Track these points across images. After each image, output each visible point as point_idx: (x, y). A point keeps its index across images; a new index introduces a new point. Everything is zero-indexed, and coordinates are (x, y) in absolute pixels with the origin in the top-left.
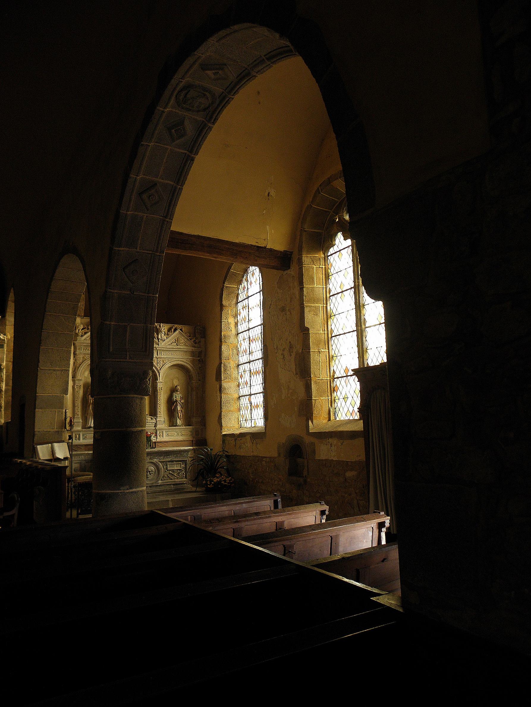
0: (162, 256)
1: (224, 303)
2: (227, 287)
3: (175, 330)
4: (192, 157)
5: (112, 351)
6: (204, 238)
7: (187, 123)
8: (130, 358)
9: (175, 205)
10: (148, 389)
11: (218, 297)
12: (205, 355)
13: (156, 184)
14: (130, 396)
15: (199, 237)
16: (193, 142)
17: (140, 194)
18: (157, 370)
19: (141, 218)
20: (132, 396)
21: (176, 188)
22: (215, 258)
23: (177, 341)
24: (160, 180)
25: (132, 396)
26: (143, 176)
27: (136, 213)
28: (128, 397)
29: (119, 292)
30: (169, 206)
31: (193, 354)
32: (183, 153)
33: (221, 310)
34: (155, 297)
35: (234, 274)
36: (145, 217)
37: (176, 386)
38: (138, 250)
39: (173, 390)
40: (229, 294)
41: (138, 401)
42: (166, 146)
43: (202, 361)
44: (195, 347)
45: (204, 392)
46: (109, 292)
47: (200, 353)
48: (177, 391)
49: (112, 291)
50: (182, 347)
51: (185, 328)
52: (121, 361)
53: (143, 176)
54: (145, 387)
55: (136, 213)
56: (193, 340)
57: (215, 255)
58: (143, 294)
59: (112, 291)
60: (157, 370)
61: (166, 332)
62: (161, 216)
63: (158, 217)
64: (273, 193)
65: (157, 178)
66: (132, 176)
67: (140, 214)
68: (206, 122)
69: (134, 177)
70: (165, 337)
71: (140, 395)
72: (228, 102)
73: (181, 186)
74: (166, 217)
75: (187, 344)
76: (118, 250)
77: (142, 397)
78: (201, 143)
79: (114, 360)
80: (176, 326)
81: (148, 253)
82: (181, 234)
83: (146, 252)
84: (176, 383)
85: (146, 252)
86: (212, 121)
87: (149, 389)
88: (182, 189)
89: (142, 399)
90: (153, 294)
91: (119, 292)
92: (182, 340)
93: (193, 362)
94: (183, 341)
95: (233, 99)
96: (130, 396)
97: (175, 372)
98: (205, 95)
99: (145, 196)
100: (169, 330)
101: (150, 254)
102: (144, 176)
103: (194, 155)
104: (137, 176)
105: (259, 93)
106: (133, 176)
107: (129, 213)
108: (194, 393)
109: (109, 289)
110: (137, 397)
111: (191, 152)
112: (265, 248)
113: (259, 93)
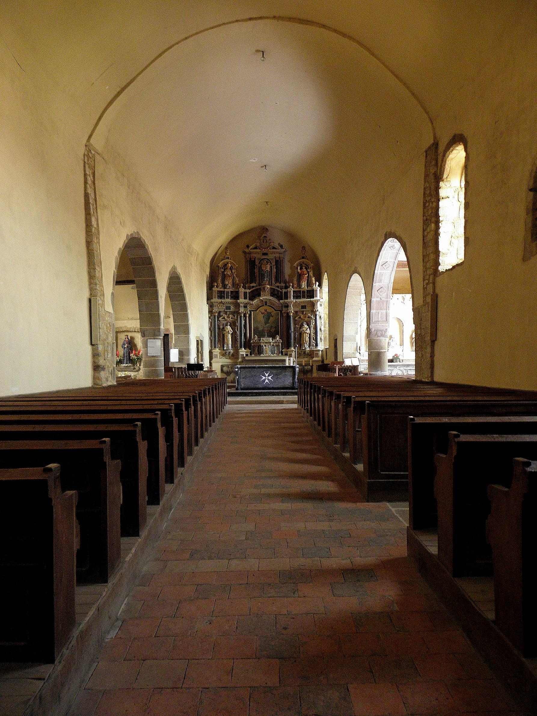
8: (381, 324)
38: (382, 284)
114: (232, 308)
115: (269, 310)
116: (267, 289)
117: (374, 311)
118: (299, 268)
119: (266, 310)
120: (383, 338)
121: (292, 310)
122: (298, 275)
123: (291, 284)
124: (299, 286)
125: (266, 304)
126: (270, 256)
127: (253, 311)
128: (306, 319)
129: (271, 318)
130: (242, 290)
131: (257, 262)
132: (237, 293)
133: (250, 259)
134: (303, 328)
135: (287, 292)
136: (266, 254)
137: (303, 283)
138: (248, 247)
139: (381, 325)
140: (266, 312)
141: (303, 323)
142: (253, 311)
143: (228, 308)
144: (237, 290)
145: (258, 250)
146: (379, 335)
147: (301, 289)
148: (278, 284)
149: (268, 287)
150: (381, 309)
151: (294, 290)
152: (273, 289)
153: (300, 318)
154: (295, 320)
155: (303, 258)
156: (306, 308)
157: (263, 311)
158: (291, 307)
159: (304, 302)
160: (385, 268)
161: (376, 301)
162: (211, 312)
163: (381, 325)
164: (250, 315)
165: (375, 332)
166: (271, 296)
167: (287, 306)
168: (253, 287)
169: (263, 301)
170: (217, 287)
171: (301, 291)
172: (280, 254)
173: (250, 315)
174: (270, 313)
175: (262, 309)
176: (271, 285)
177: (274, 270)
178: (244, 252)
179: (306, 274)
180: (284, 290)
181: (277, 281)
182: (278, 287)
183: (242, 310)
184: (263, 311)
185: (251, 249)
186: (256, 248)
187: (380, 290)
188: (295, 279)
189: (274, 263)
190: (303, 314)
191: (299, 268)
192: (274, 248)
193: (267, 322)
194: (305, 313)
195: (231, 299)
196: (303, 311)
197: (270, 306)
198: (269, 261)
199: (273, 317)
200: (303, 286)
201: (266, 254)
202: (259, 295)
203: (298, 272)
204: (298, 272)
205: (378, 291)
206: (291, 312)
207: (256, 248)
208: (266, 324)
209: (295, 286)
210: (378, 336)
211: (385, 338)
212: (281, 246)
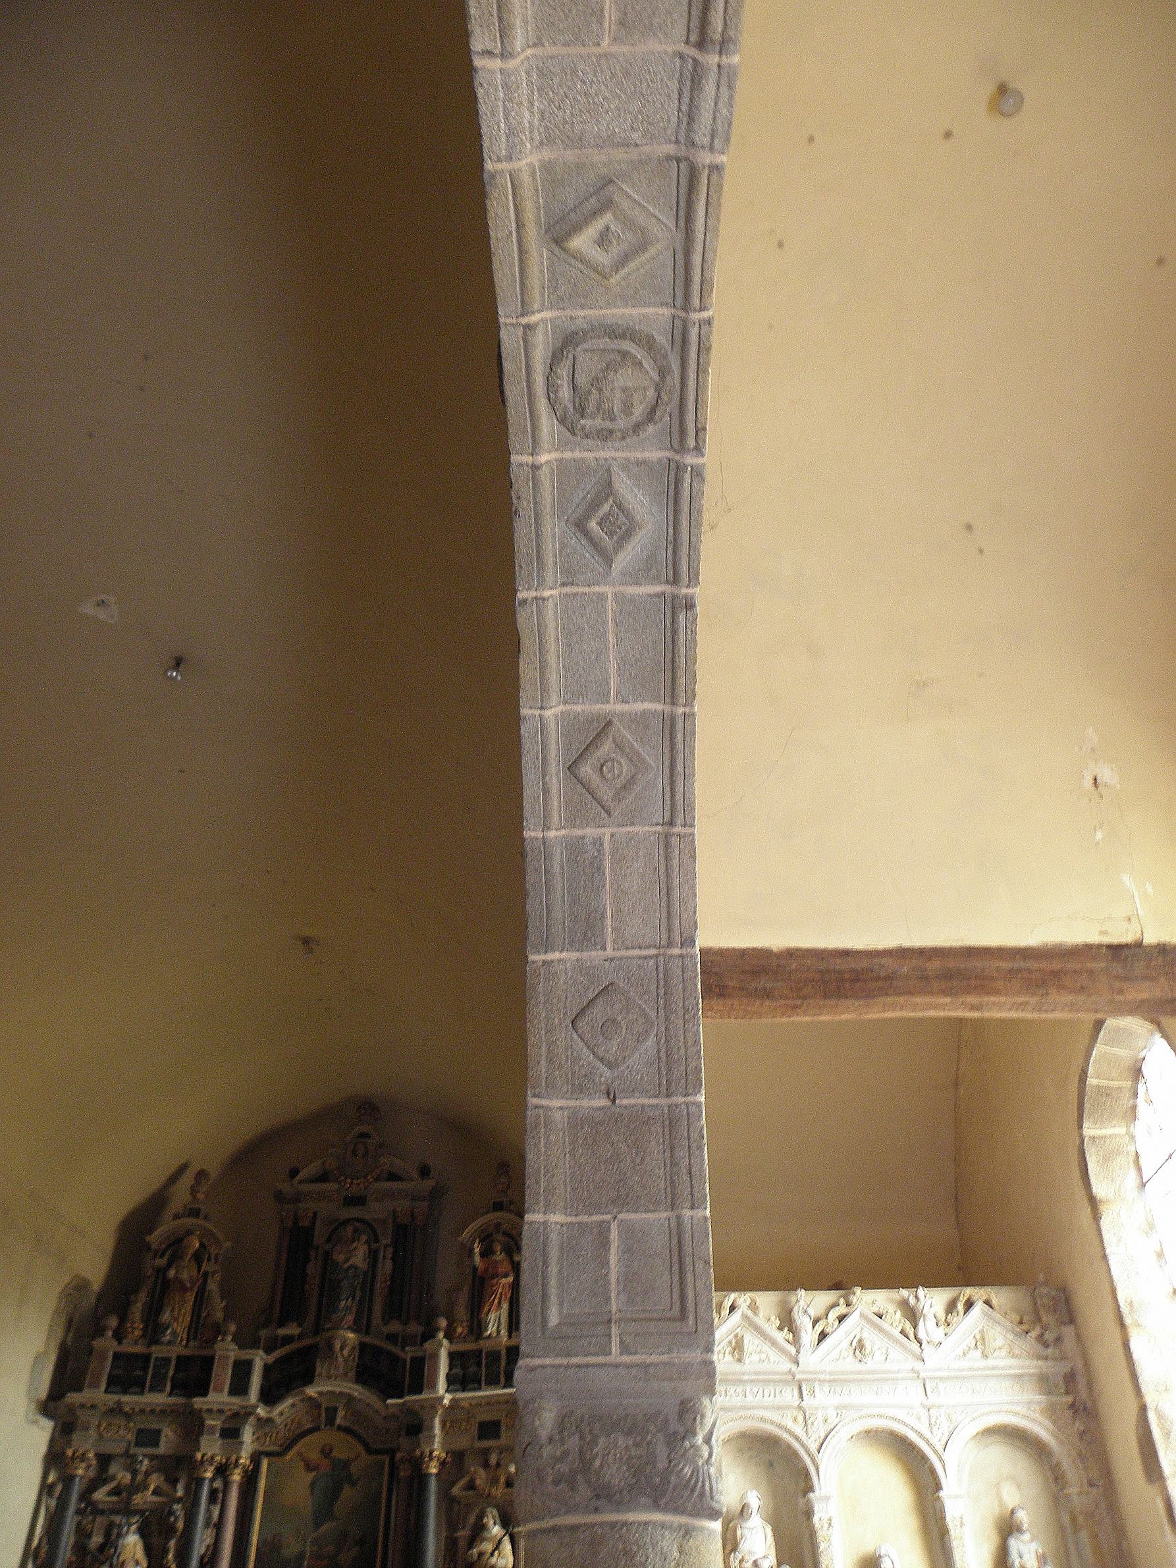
0: (693, 957)
1: (1099, 1189)
2: (1093, 1139)
3: (969, 1305)
4: (686, 597)
5: (559, 1324)
6: (921, 952)
7: (623, 485)
8: (625, 1349)
9: (688, 776)
10: (703, 1485)
11: (1076, 1173)
12: (1090, 1385)
13: (609, 723)
14: (631, 1517)
15: (903, 953)
16: (671, 547)
17: (572, 768)
18: (936, 1452)
19: (595, 844)
20: (643, 1517)
21: (673, 719)
22: (974, 1008)
23: (981, 1341)
24: (620, 707)
25: (643, 1517)
26: (561, 708)
27: (578, 832)
28: (625, 1524)
29: (572, 1103)
30: (672, 783)
31: (1044, 1383)
32: (658, 595)
33: (1096, 1216)
34: (694, 1103)
35: (1105, 1092)
36: (607, 838)
37: (1013, 1512)
38: (610, 952)
39: (1007, 1528)
40: (1107, 1159)
41: (669, 1543)
42: (596, 589)
43: (1085, 1408)
44: (1046, 1358)
45: (1120, 1531)
46: (537, 1107)
47: (1070, 1379)
48: (1019, 1530)
49: (544, 1102)
50: (1002, 1363)
51: (1000, 1296)
52: (588, 1366)
53: (561, 708)
54: (693, 1472)
55: (578, 832)
56: (1034, 1334)
57: (972, 999)
58: (654, 1101)
59: (544, 1102)
60: (936, 1452)
61: (942, 1315)
62: (657, 824)
63: (648, 828)
64: (1107, 775)
65: (608, 702)
66: (525, 711)
67: (590, 832)
68: (677, 457)
69: (533, 716)
70: (938, 1334)
71: (682, 1512)
72: (704, 348)
73: (685, 706)
74: (671, 823)
75: (1017, 1352)
76: (544, 962)
77: (686, 1525)
78: (693, 539)
79: (564, 1361)
80: (968, 1291)
81: (645, 958)
82: (846, 953)
83: (637, 952)
84: (1011, 1497)
85: (637, 952)
86: (691, 443)
87: (710, 1484)
88: (693, 714)
89: (687, 1532)
90: (686, 1095)
91: (572, 1103)
92: (999, 1337)
93: (1051, 1411)
94: (1000, 1341)
95: (709, 322)
96: (631, 1517)
97: (999, 1456)
98: (624, 355)
99: (587, 770)
100: (951, 1308)
101: (650, 957)
102: (568, 707)
103: (688, 586)
104: (542, 708)
105: (969, 527)
106: (530, 712)
107: (551, 834)
108: (1084, 1535)
109: (534, 1096)
110: (663, 1526)
111: (675, 581)
112: (1139, 944)
113: (969, 527)
114: (169, 1440)
115: (344, 1447)
116: (342, 1348)
117: (556, 1218)
118: (477, 1250)
119: (326, 1452)
120: (658, 1517)
121: (437, 1444)
122: (474, 1279)
123: (443, 1323)
124: (477, 1328)
125: (330, 1421)
126: (376, 1210)
127: (268, 1454)
128: (499, 1492)
129: (347, 1492)
130: (228, 1351)
131: (320, 1235)
132: (208, 1363)
133: (295, 1223)
134: (483, 1540)
135: (423, 1359)
136: (358, 1201)
137: (492, 1316)
138: (294, 1173)
139: (626, 1359)
140: (326, 1462)
141: (481, 1516)
142: (268, 1454)
143: (148, 1438)
144: (206, 1352)
145: (330, 1186)
146: (615, 1474)
147: (483, 1344)
148: (395, 1327)
149: (346, 1339)
150: (623, 1201)
151: (456, 1348)
152: (374, 1347)
153: (471, 1486)
154: (446, 1498)
155: (498, 1207)
156: (498, 1437)
157: (314, 1456)
158: (431, 1428)
159: (489, 1403)
160: (606, 794)
161: (577, 1121)
162: (54, 1458)
163: (626, 1359)
164: (250, 1479)
165: (573, 1442)
166: (357, 1381)
167: (416, 1427)
168: (288, 1340)
169: (319, 1406)
170: (119, 1336)
171: (481, 1351)
172: (414, 1199)
173: (250, 1479)
174: (346, 1464)
175: (310, 1447)
176: (367, 1333)
177: (386, 1267)
178: (279, 1197)
179: (506, 1276)
180: (410, 1353)
181: (394, 1310)
182: (392, 1338)
183: (211, 1447)
184: (314, 1456)
185: (300, 1182)
186: (323, 1178)
187: (598, 1012)
188: (462, 1299)
189: (386, 1240)
190: (486, 1465)
191: (477, 1250)
192: (393, 1177)
193: (322, 1514)
194: (493, 1459)
195: (170, 1394)
196: (486, 1452)
197: (347, 1430)
198: (370, 1228)
199: (353, 1483)
200: (491, 1329)
201: (358, 1201)
202: (308, 1378)
203: (474, 1267)
204: (475, 1269)
205: (580, 1024)
206: (431, 1458)
207: (323, 1178)
208: (317, 1526)
209: (460, 1330)
210: (604, 1495)
211: (684, 1519)
212: (425, 1172)
